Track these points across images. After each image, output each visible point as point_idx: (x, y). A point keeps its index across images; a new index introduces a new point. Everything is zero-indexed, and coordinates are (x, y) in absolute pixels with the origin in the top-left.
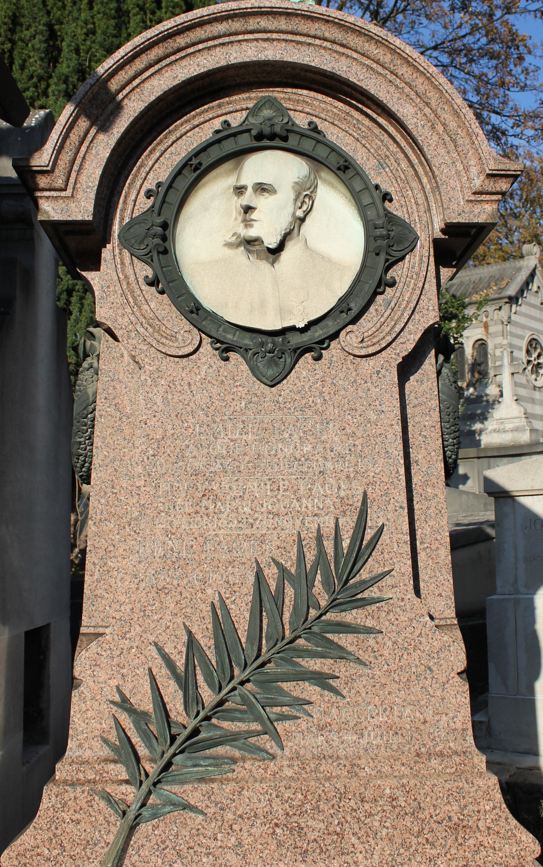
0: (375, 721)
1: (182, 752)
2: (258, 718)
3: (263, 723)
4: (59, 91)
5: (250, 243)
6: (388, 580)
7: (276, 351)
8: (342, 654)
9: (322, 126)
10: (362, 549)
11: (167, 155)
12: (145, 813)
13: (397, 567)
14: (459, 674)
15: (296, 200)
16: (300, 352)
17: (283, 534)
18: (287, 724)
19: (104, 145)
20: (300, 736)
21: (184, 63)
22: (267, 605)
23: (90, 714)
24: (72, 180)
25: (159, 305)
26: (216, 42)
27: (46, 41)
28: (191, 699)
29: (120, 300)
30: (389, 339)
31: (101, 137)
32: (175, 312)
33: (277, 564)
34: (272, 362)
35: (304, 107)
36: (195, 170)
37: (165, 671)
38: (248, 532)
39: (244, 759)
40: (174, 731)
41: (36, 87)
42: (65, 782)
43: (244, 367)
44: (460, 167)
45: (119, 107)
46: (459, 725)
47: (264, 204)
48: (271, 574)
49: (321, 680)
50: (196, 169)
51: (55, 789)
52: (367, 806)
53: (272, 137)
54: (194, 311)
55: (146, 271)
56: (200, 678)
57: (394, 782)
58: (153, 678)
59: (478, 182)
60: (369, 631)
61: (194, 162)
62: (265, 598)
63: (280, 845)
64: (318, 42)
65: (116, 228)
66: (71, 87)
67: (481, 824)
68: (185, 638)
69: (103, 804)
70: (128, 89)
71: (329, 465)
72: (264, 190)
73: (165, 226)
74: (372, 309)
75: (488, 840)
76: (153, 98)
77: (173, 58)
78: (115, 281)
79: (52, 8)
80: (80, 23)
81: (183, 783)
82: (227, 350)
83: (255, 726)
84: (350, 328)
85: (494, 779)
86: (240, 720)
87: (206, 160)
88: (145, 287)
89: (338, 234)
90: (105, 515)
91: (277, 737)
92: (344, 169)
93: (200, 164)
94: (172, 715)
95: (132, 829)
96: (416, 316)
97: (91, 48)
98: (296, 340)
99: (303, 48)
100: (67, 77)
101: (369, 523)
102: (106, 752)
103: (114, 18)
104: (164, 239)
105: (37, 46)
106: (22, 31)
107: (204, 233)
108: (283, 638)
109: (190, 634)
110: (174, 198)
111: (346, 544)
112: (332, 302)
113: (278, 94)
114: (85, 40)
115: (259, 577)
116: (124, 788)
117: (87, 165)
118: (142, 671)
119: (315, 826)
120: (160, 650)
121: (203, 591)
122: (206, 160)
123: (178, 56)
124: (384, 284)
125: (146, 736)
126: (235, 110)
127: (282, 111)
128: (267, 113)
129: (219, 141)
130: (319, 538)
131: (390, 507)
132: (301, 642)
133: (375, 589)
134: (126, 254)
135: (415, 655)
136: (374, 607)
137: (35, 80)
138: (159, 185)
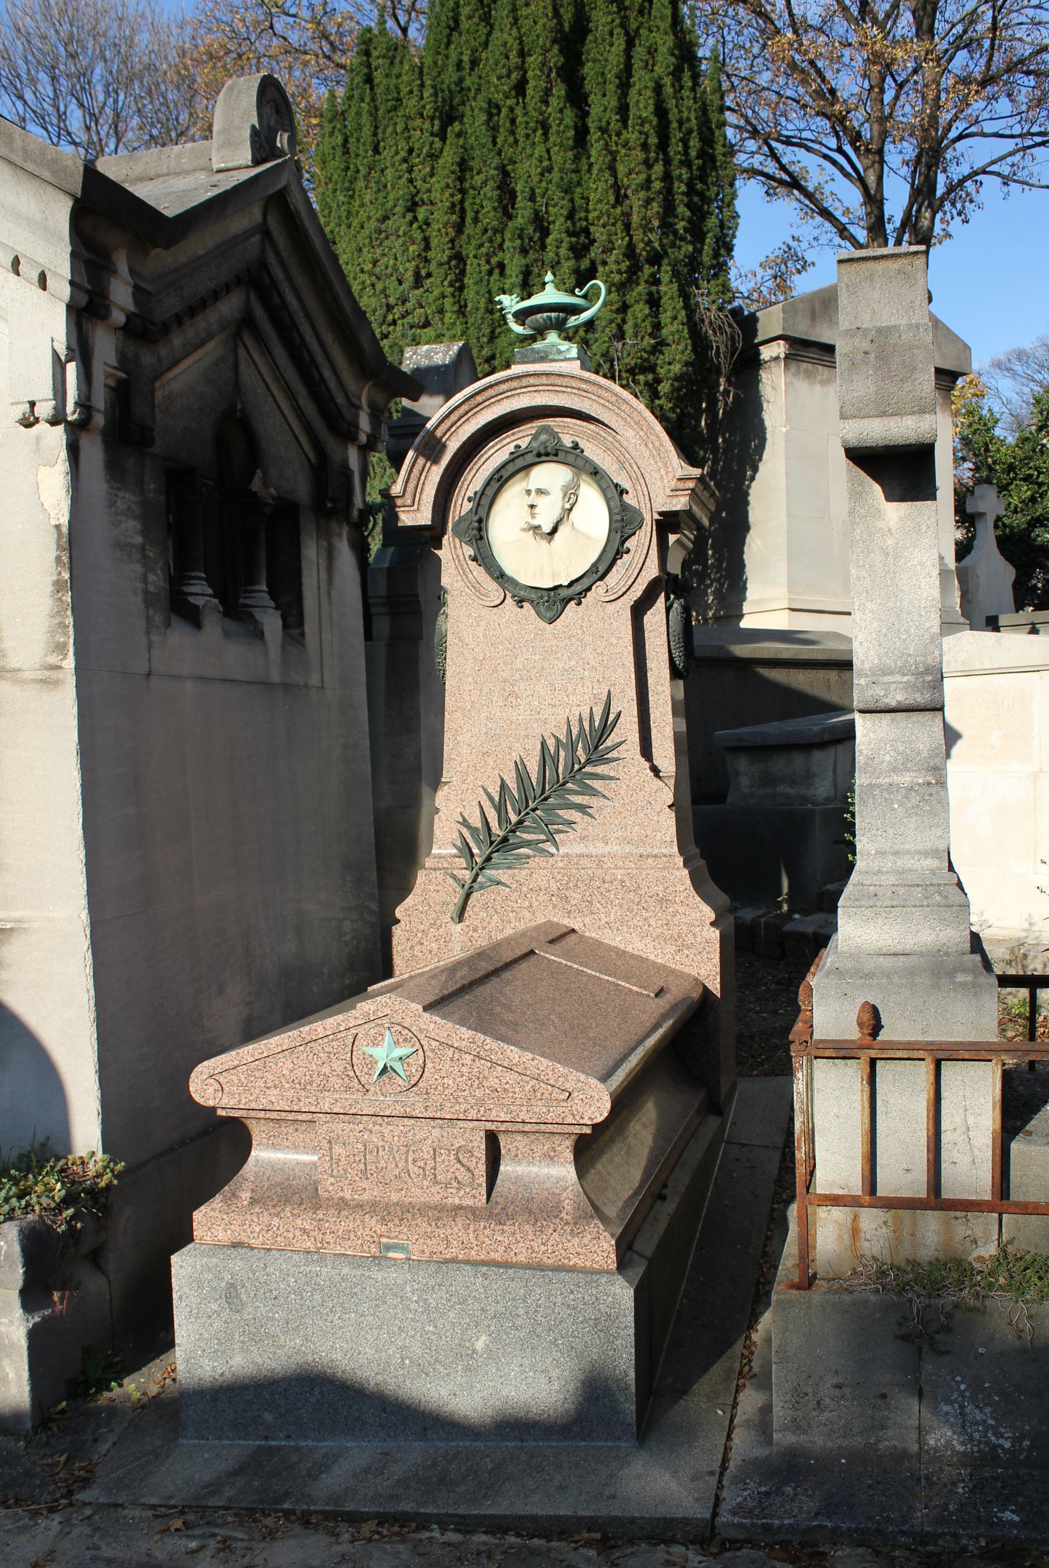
0: (615, 835)
1: (497, 851)
2: (543, 832)
3: (546, 835)
4: (514, 248)
5: (536, 528)
6: (623, 747)
7: (553, 601)
8: (594, 793)
9: (582, 444)
10: (606, 727)
11: (480, 471)
12: (475, 885)
13: (629, 738)
14: (669, 807)
15: (564, 498)
16: (567, 601)
17: (558, 718)
18: (562, 835)
19: (436, 473)
20: (569, 845)
21: (483, 412)
22: (549, 762)
23: (445, 829)
24: (417, 499)
25: (478, 572)
26: (503, 396)
27: (499, 188)
28: (503, 818)
29: (455, 572)
30: (624, 589)
31: (434, 468)
32: (489, 579)
33: (555, 736)
34: (549, 608)
35: (568, 432)
36: (499, 480)
37: (488, 803)
38: (537, 717)
39: (534, 856)
40: (493, 839)
41: (491, 241)
42: (431, 869)
43: (533, 612)
44: (663, 472)
45: (444, 447)
46: (668, 839)
47: (541, 502)
48: (551, 743)
49: (582, 809)
50: (498, 481)
51: (425, 872)
52: (606, 885)
53: (547, 454)
54: (500, 577)
55: (469, 551)
56: (509, 807)
57: (623, 871)
58: (481, 807)
59: (673, 484)
60: (611, 778)
61: (496, 476)
62: (547, 758)
63: (554, 907)
64: (569, 390)
65: (450, 525)
66: (527, 241)
67: (677, 899)
68: (499, 783)
69: (452, 881)
70: (448, 434)
71: (586, 673)
72: (542, 493)
73: (480, 521)
74: (614, 569)
75: (681, 909)
76: (465, 439)
77: (475, 410)
78: (452, 555)
79: (503, 146)
80: (534, 161)
81: (498, 869)
82: (521, 601)
83: (542, 837)
84: (598, 583)
85: (686, 872)
86: (533, 833)
87: (505, 474)
88: (470, 562)
89: (593, 517)
90: (455, 708)
91: (555, 844)
92: (596, 473)
93: (501, 477)
94: (493, 830)
95: (468, 896)
96: (643, 573)
97: (547, 190)
98: (564, 593)
99: (560, 395)
100: (522, 230)
101: (612, 710)
102: (455, 851)
103: (572, 149)
104: (480, 530)
105: (489, 195)
106: (472, 177)
107: (506, 524)
108: (558, 782)
109: (502, 780)
110: (485, 501)
111: (597, 724)
112: (586, 567)
113: (550, 422)
114: (541, 181)
115: (543, 744)
116: (464, 871)
117: (426, 487)
118: (475, 803)
119: (575, 896)
120: (485, 790)
121: (510, 754)
122: (505, 474)
123: (478, 409)
124: (619, 554)
125: (479, 843)
126: (522, 437)
127: (555, 435)
128: (543, 437)
129: (513, 460)
130: (581, 720)
131: (625, 700)
132: (569, 785)
133: (615, 752)
134: (457, 541)
135: (641, 794)
136: (615, 763)
137: (490, 233)
138: (476, 493)
